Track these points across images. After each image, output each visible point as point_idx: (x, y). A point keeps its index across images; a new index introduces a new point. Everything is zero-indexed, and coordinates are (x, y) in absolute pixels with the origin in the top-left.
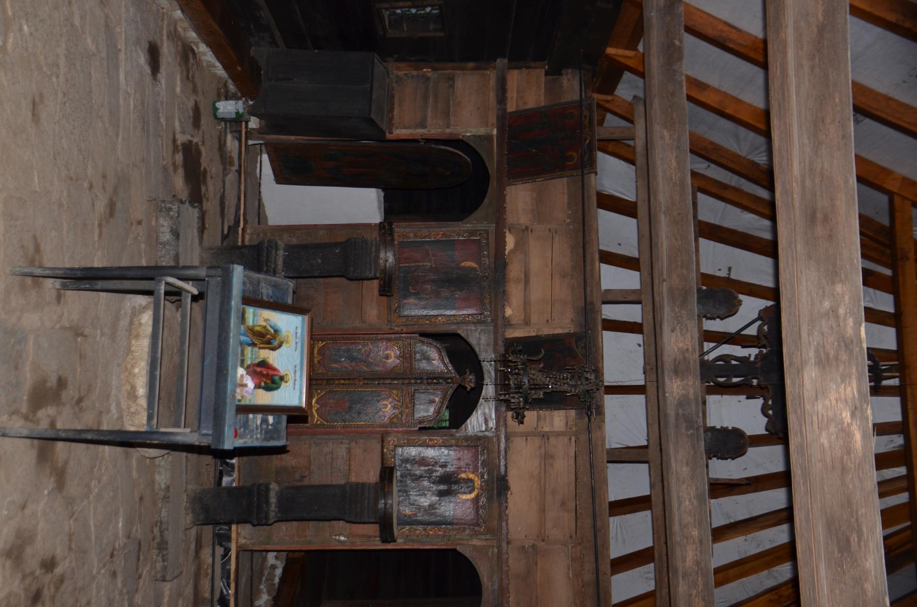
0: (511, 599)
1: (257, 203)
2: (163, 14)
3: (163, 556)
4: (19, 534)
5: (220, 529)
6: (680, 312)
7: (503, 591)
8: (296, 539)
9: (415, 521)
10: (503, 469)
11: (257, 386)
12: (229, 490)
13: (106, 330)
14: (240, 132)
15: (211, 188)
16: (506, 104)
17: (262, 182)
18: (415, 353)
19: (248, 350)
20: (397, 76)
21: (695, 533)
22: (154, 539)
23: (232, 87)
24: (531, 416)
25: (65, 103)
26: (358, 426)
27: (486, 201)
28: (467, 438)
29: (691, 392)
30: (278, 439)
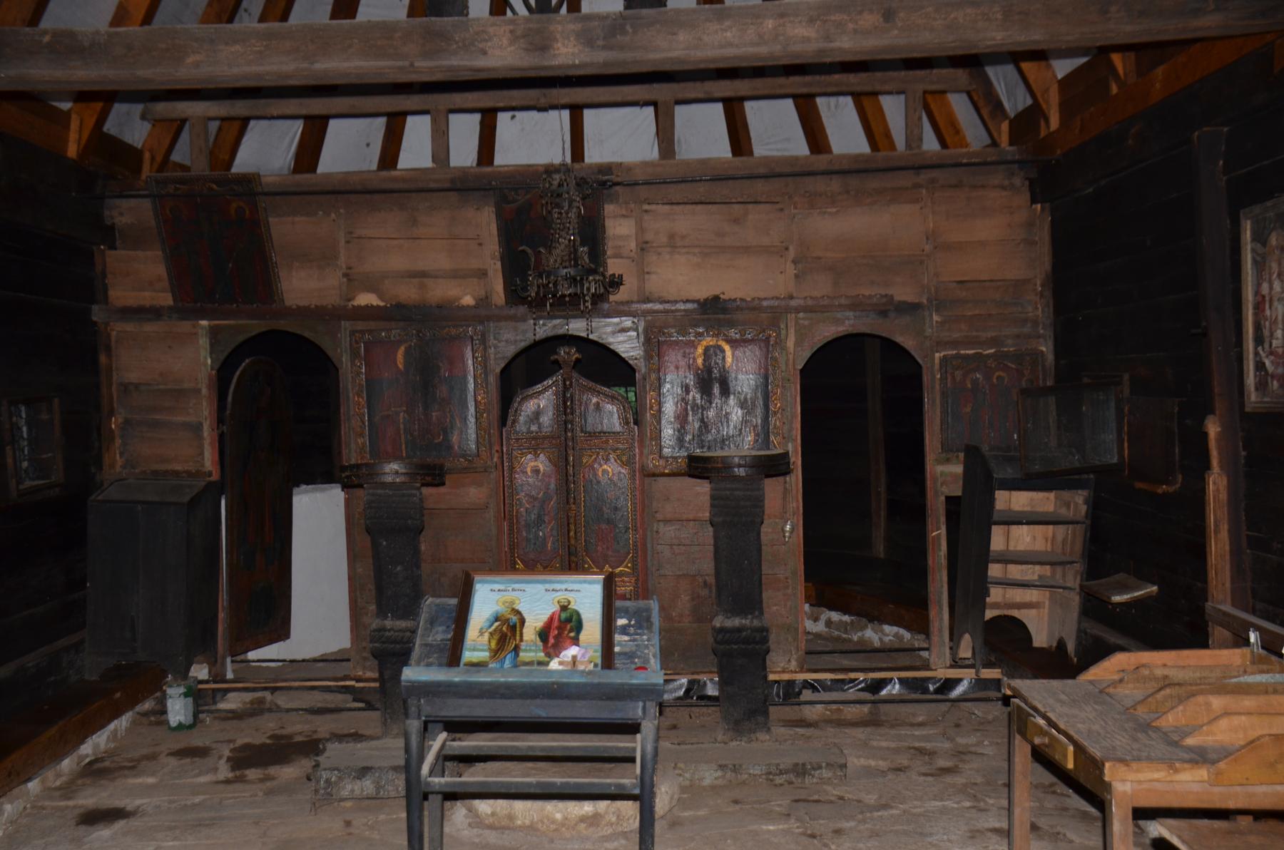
0: (867, 293)
1: (321, 664)
2: (33, 807)
3: (814, 769)
5: (778, 696)
6: (457, 43)
7: (856, 305)
8: (790, 591)
9: (763, 427)
10: (690, 306)
11: (576, 641)
12: (723, 684)
14: (214, 690)
15: (298, 728)
16: (162, 308)
17: (289, 657)
18: (529, 432)
20: (124, 467)
21: (770, 24)
22: (791, 783)
23: (147, 705)
24: (614, 267)
26: (634, 511)
27: (307, 334)
28: (648, 356)
29: (571, 26)
30: (648, 610)
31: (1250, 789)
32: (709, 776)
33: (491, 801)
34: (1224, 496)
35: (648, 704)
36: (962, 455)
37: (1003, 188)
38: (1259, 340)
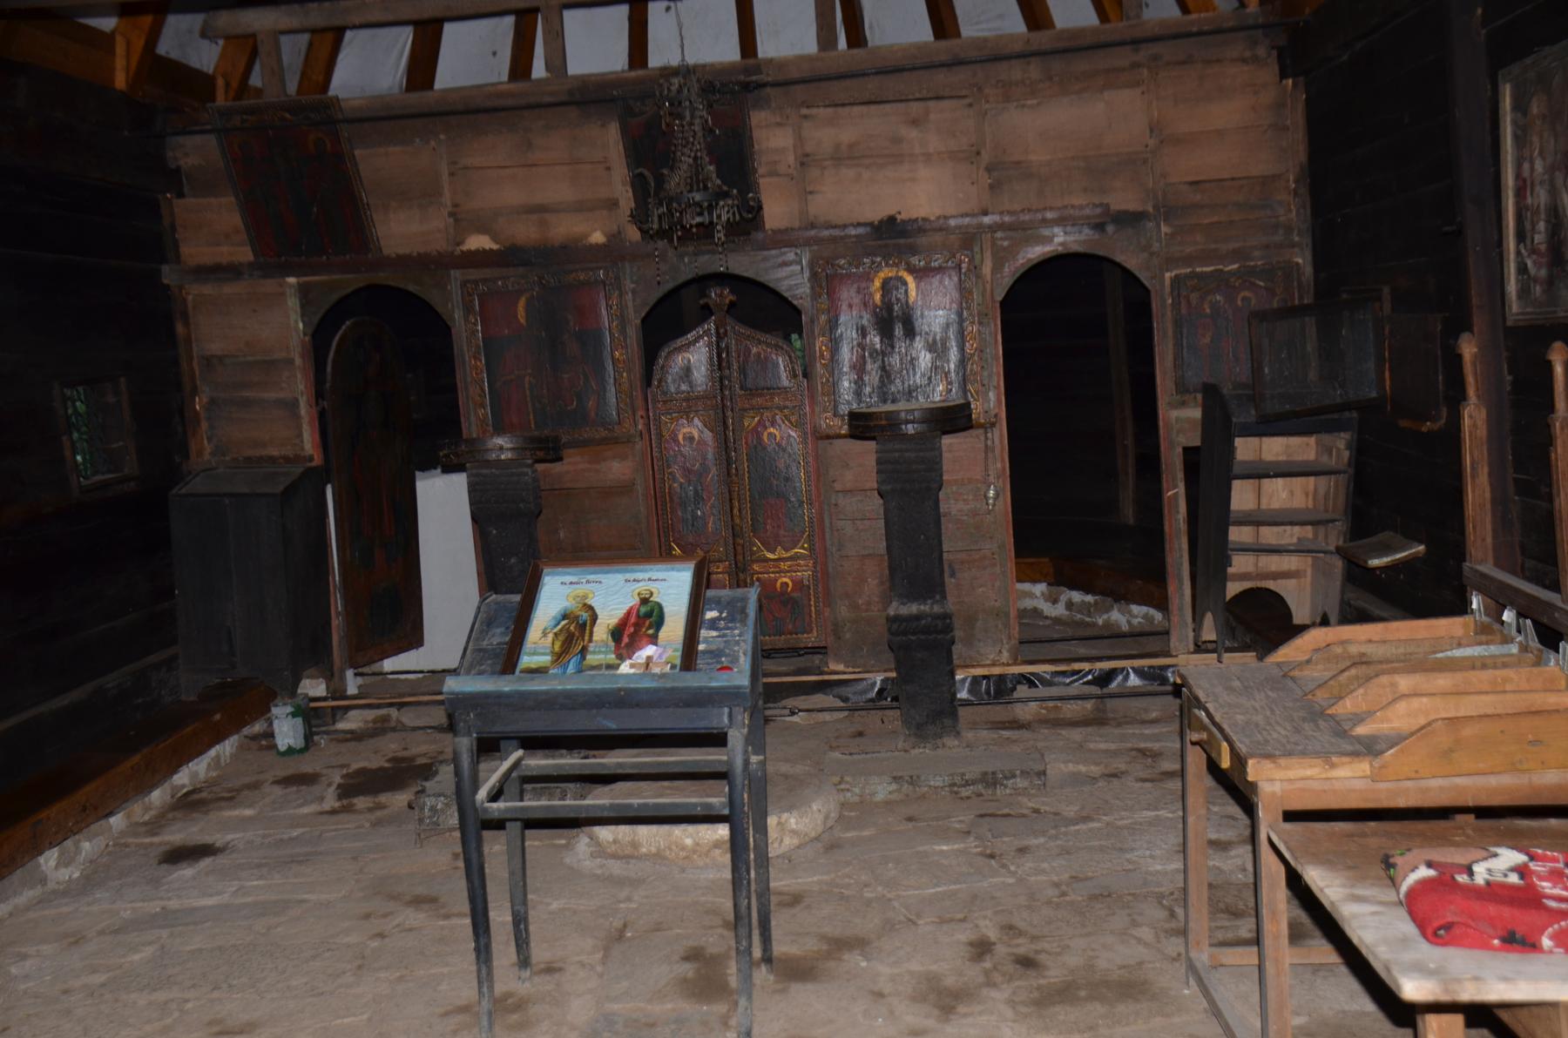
3: (1006, 778)
4: (918, 998)
8: (998, 570)
10: (860, 230)
11: (654, 640)
13: (623, 894)
15: (423, 748)
16: (241, 264)
19: (591, 659)
20: (213, 454)
22: (980, 795)
23: (258, 727)
25: (230, 986)
27: (411, 288)
28: (815, 295)
30: (745, 600)
31: (1423, 783)
32: (882, 790)
33: (612, 828)
34: (1482, 432)
35: (735, 710)
36: (1199, 396)
37: (1244, 61)
38: (1521, 236)
